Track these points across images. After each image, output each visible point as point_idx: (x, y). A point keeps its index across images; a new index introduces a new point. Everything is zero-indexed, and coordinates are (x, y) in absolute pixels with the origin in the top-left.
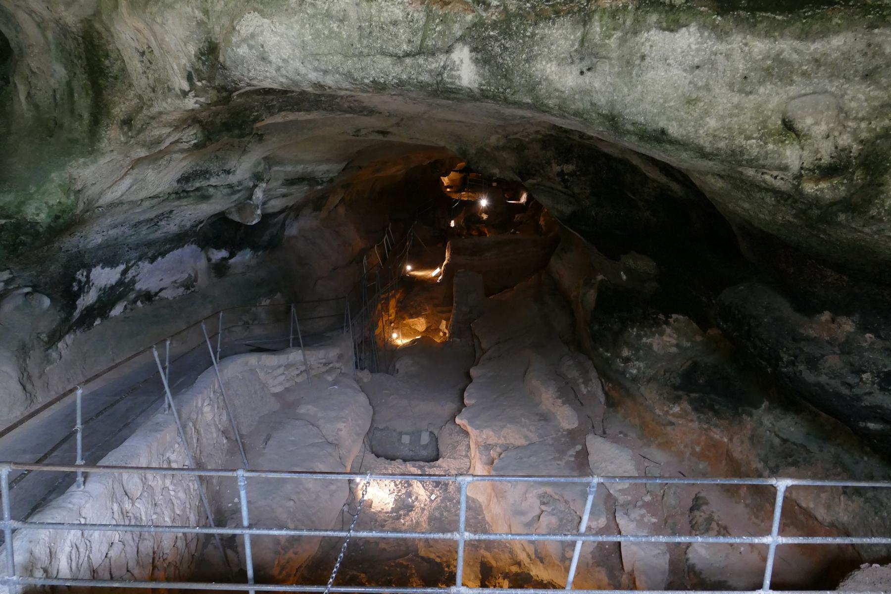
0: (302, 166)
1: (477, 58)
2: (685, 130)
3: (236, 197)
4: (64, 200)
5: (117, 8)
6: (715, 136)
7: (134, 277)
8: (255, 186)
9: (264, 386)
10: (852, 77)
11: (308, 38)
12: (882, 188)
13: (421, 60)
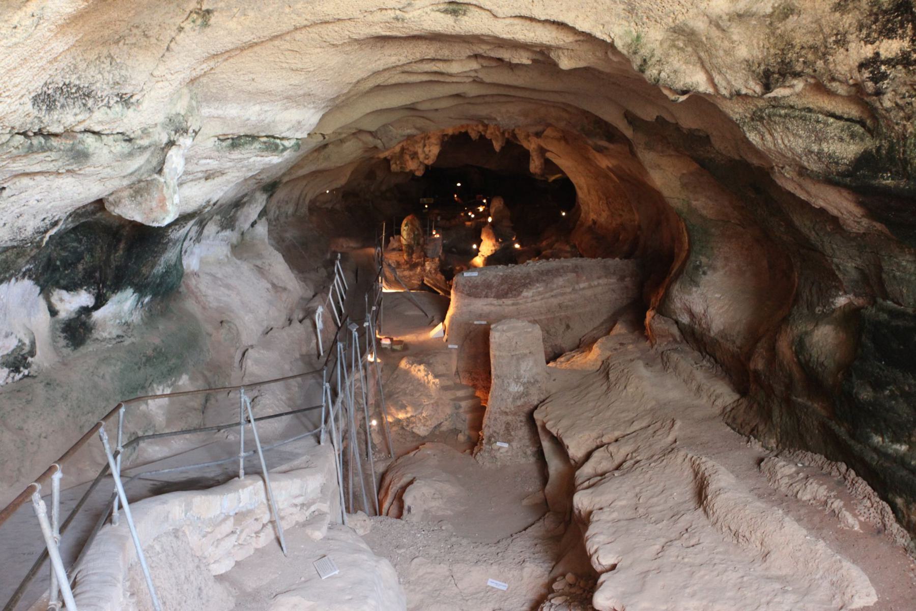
0: (257, 108)
8: (171, 143)
9: (201, 563)
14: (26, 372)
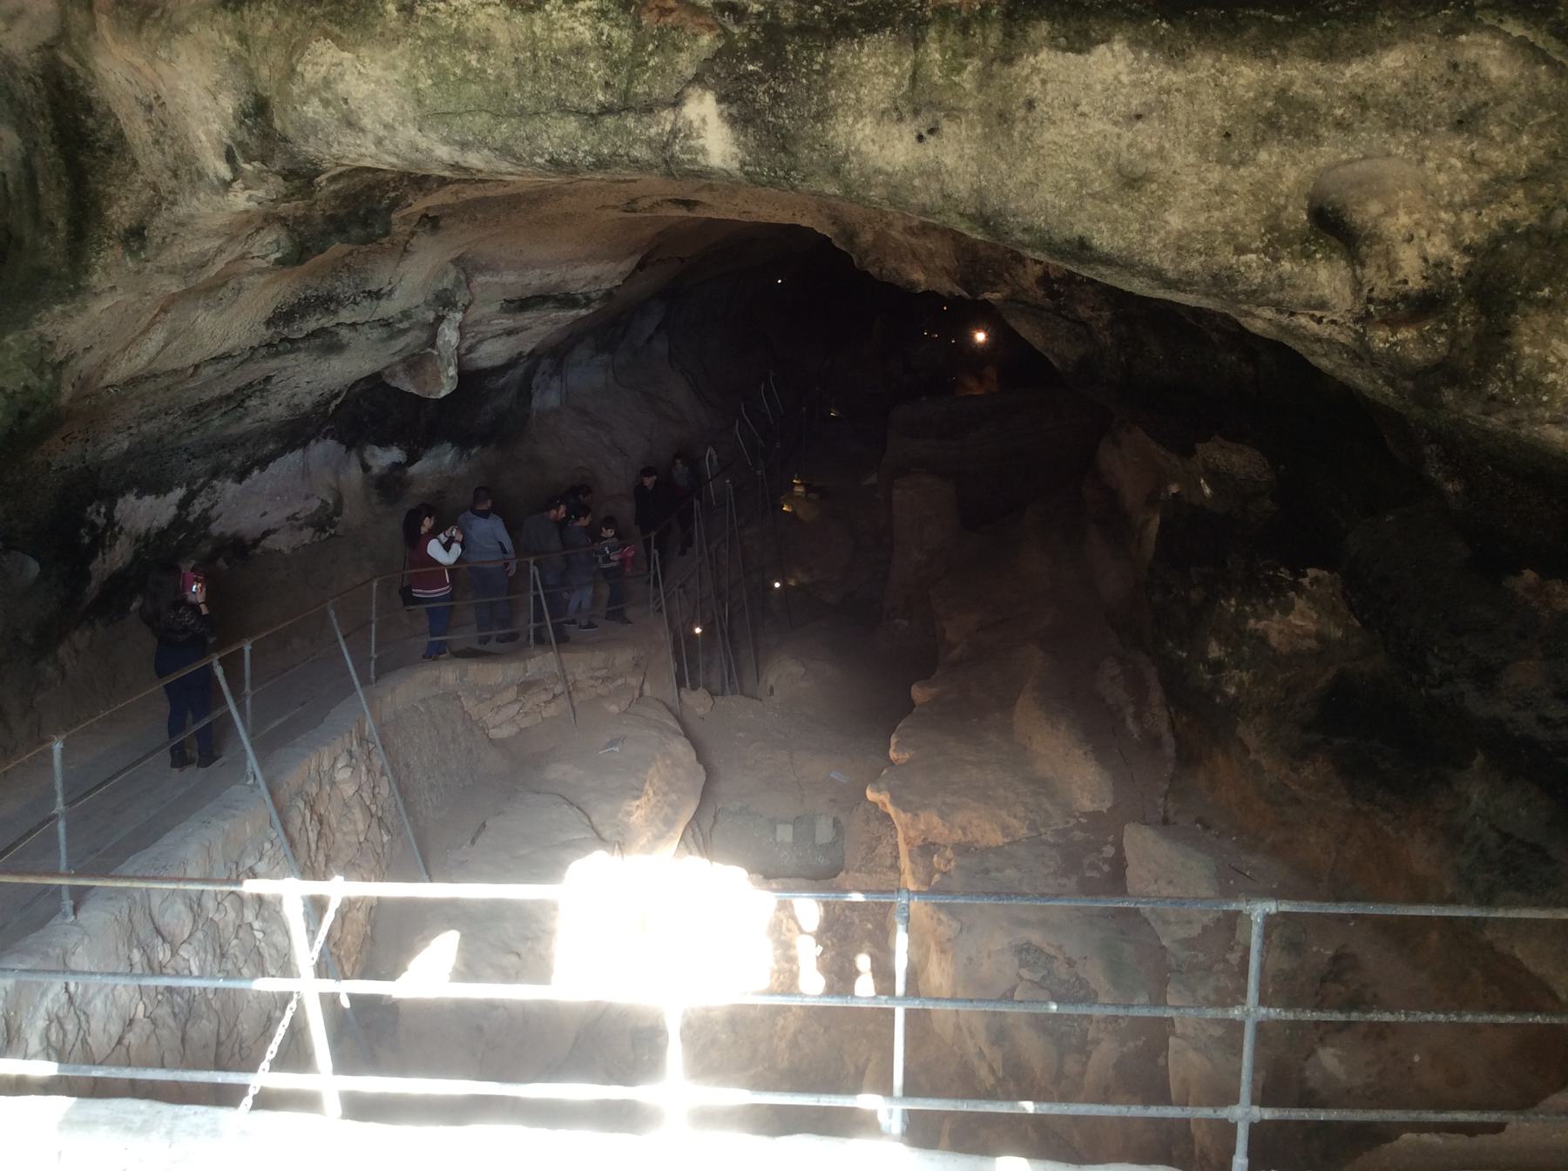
1: (730, 115)
2: (1124, 239)
3: (401, 343)
4: (34, 381)
5: (95, 30)
6: (1180, 248)
7: (206, 510)
8: (440, 319)
10: (1431, 126)
11: (425, 83)
12: (1506, 340)
13: (630, 122)
14: (333, 531)
